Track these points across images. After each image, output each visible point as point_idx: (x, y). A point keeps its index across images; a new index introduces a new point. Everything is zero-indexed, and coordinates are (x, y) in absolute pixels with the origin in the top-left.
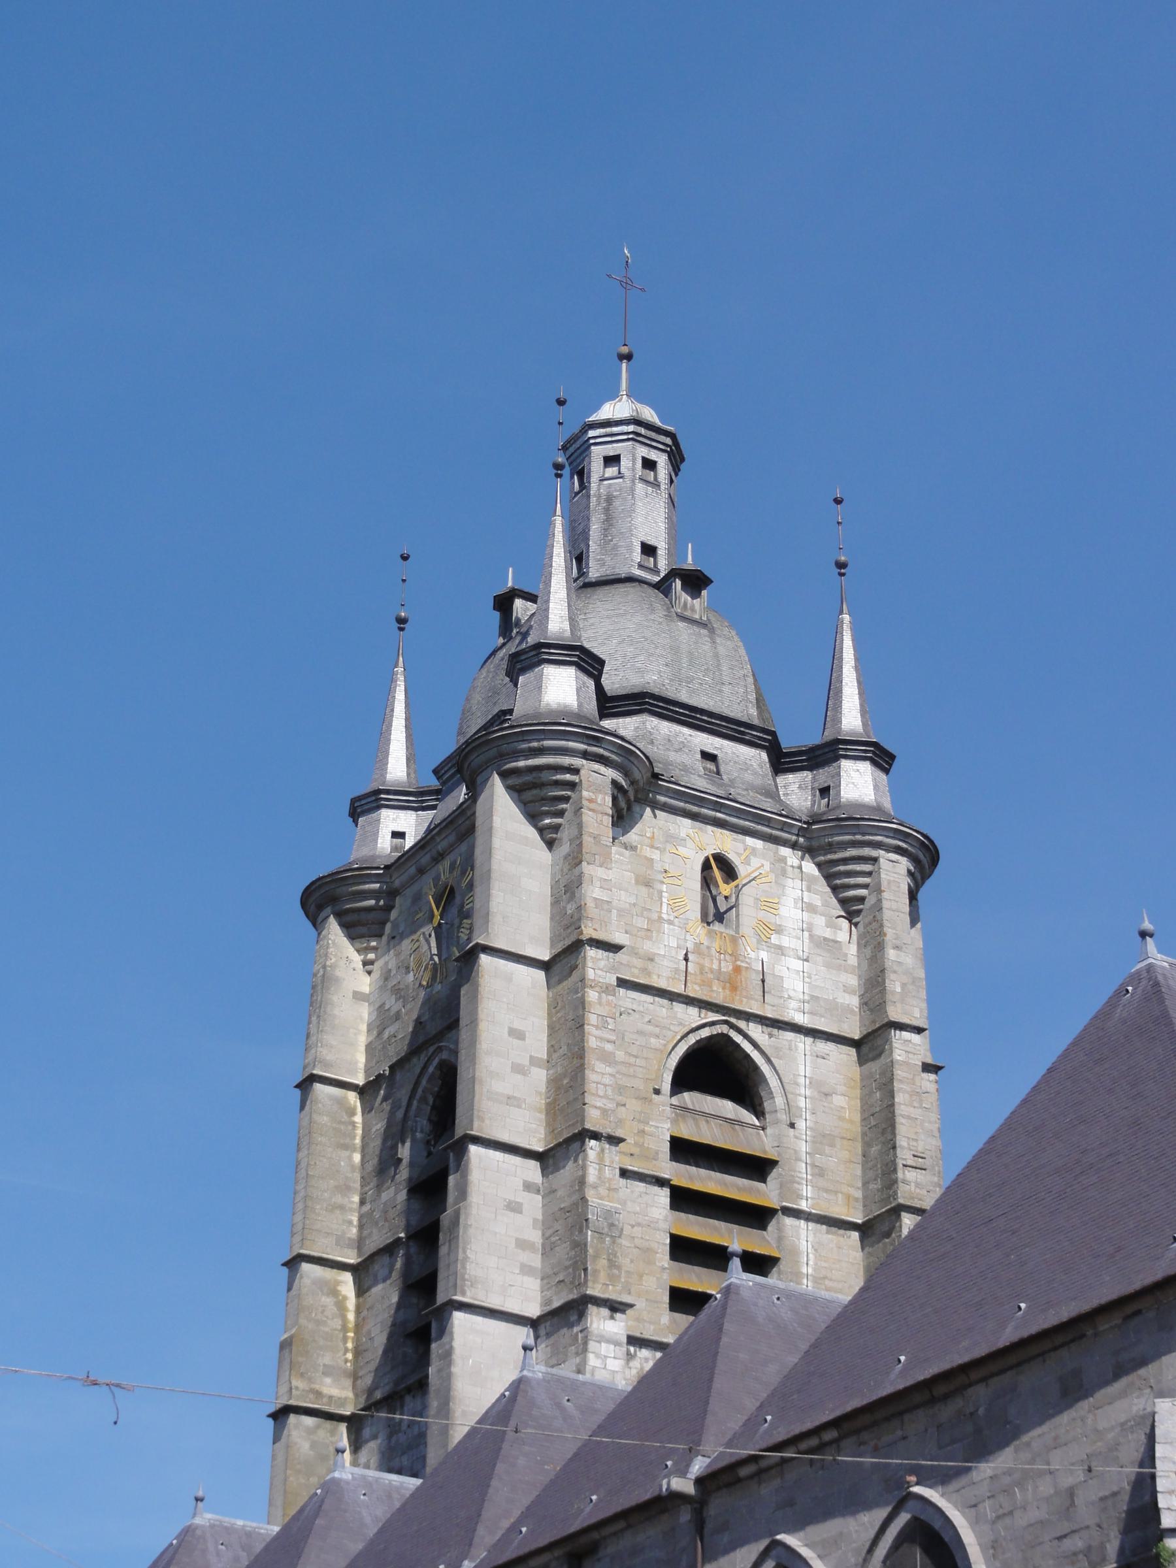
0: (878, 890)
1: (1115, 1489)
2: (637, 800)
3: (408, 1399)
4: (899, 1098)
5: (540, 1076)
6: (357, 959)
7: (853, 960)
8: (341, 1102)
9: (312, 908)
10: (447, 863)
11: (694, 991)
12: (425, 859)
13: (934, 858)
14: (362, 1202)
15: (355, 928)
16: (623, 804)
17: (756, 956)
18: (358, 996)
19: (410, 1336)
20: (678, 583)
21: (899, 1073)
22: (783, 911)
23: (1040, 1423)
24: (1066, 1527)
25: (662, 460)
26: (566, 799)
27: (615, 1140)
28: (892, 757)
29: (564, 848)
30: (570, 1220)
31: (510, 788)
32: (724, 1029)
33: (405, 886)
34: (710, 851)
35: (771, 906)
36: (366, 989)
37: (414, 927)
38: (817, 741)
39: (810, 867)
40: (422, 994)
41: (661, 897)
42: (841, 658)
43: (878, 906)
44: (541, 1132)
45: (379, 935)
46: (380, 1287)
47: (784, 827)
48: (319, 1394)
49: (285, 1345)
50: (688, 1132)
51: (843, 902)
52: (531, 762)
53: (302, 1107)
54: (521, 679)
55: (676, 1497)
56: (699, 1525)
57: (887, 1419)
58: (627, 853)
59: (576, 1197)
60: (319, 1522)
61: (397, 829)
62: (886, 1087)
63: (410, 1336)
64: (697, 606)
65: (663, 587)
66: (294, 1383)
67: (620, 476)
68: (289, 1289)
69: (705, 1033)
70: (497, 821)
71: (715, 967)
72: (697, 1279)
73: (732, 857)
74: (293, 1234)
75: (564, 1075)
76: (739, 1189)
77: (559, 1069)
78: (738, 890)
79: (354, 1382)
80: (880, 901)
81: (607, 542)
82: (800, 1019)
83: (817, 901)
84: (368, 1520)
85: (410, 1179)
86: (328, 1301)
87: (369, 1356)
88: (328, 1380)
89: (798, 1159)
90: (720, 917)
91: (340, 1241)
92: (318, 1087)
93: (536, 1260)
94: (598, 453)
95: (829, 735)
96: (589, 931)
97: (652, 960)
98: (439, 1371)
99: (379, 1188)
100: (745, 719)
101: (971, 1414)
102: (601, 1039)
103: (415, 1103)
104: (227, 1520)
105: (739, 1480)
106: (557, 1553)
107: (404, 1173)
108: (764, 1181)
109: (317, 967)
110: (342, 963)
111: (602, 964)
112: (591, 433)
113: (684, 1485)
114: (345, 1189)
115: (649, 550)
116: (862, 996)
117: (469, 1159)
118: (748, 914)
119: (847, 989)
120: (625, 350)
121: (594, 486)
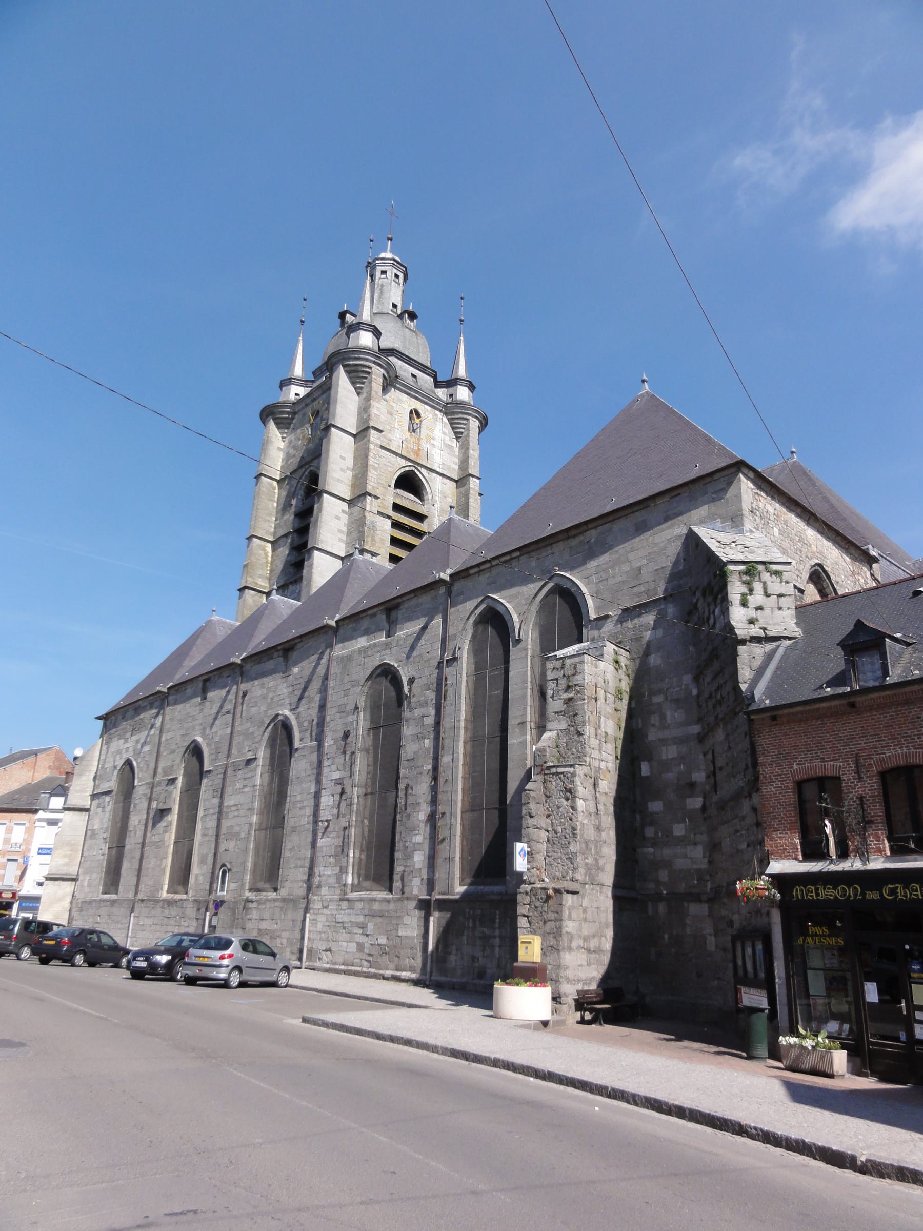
0: (468, 430)
1: (664, 565)
2: (389, 385)
3: (290, 586)
4: (470, 500)
5: (350, 474)
6: (280, 436)
7: (457, 454)
8: (271, 485)
9: (264, 417)
10: (316, 402)
11: (404, 454)
12: (308, 400)
13: (486, 424)
14: (276, 520)
15: (280, 424)
16: (385, 384)
17: (425, 446)
18: (279, 449)
19: (292, 565)
20: (406, 316)
21: (471, 491)
22: (435, 432)
23: (625, 542)
24: (636, 583)
25: (401, 276)
26: (366, 378)
27: (377, 497)
28: (475, 388)
29: (364, 395)
30: (359, 524)
31: (346, 371)
32: (413, 469)
33: (299, 411)
34: (413, 408)
35: (432, 430)
36: (282, 447)
37: (302, 425)
38: (449, 379)
39: (445, 419)
40: (304, 447)
41: (395, 420)
42: (460, 352)
43: (468, 435)
44: (349, 494)
45: (288, 428)
46: (281, 549)
47: (438, 404)
48: (256, 584)
49: (245, 566)
50: (398, 502)
51: (455, 433)
52: (354, 362)
53: (257, 485)
54: (351, 335)
55: (441, 581)
56: (449, 593)
57: (545, 547)
58: (385, 402)
59: (361, 516)
60: (267, 612)
61: (297, 393)
62: (467, 496)
63: (292, 565)
64: (412, 325)
65: (400, 316)
66: (248, 579)
67: (386, 278)
68: (248, 547)
69: (407, 469)
70: (340, 382)
71: (412, 447)
72: (399, 552)
73: (420, 411)
74: (250, 528)
75: (359, 474)
76: (415, 524)
77: (357, 472)
78: (421, 421)
79: (269, 582)
80: (468, 434)
81: (380, 301)
82: (438, 470)
83: (447, 431)
84: (284, 614)
85: (295, 512)
86: (262, 552)
87: (275, 572)
88: (260, 580)
89: (435, 517)
90: (414, 431)
91: (267, 532)
92: (263, 478)
93: (344, 537)
94: (379, 269)
95: (454, 377)
96: (371, 424)
97: (391, 441)
98: (308, 571)
99: (283, 515)
100: (426, 365)
101: (587, 542)
102: (374, 462)
103: (299, 485)
104: (224, 619)
105: (470, 575)
106: (381, 608)
107: (293, 509)
108: (422, 523)
109: (264, 437)
110: (274, 436)
111: (376, 436)
112: (377, 262)
113: (445, 576)
114: (270, 515)
115: (395, 306)
116: (459, 466)
117: (323, 500)
118: (424, 431)
119: (454, 463)
120: (390, 236)
121: (377, 280)
